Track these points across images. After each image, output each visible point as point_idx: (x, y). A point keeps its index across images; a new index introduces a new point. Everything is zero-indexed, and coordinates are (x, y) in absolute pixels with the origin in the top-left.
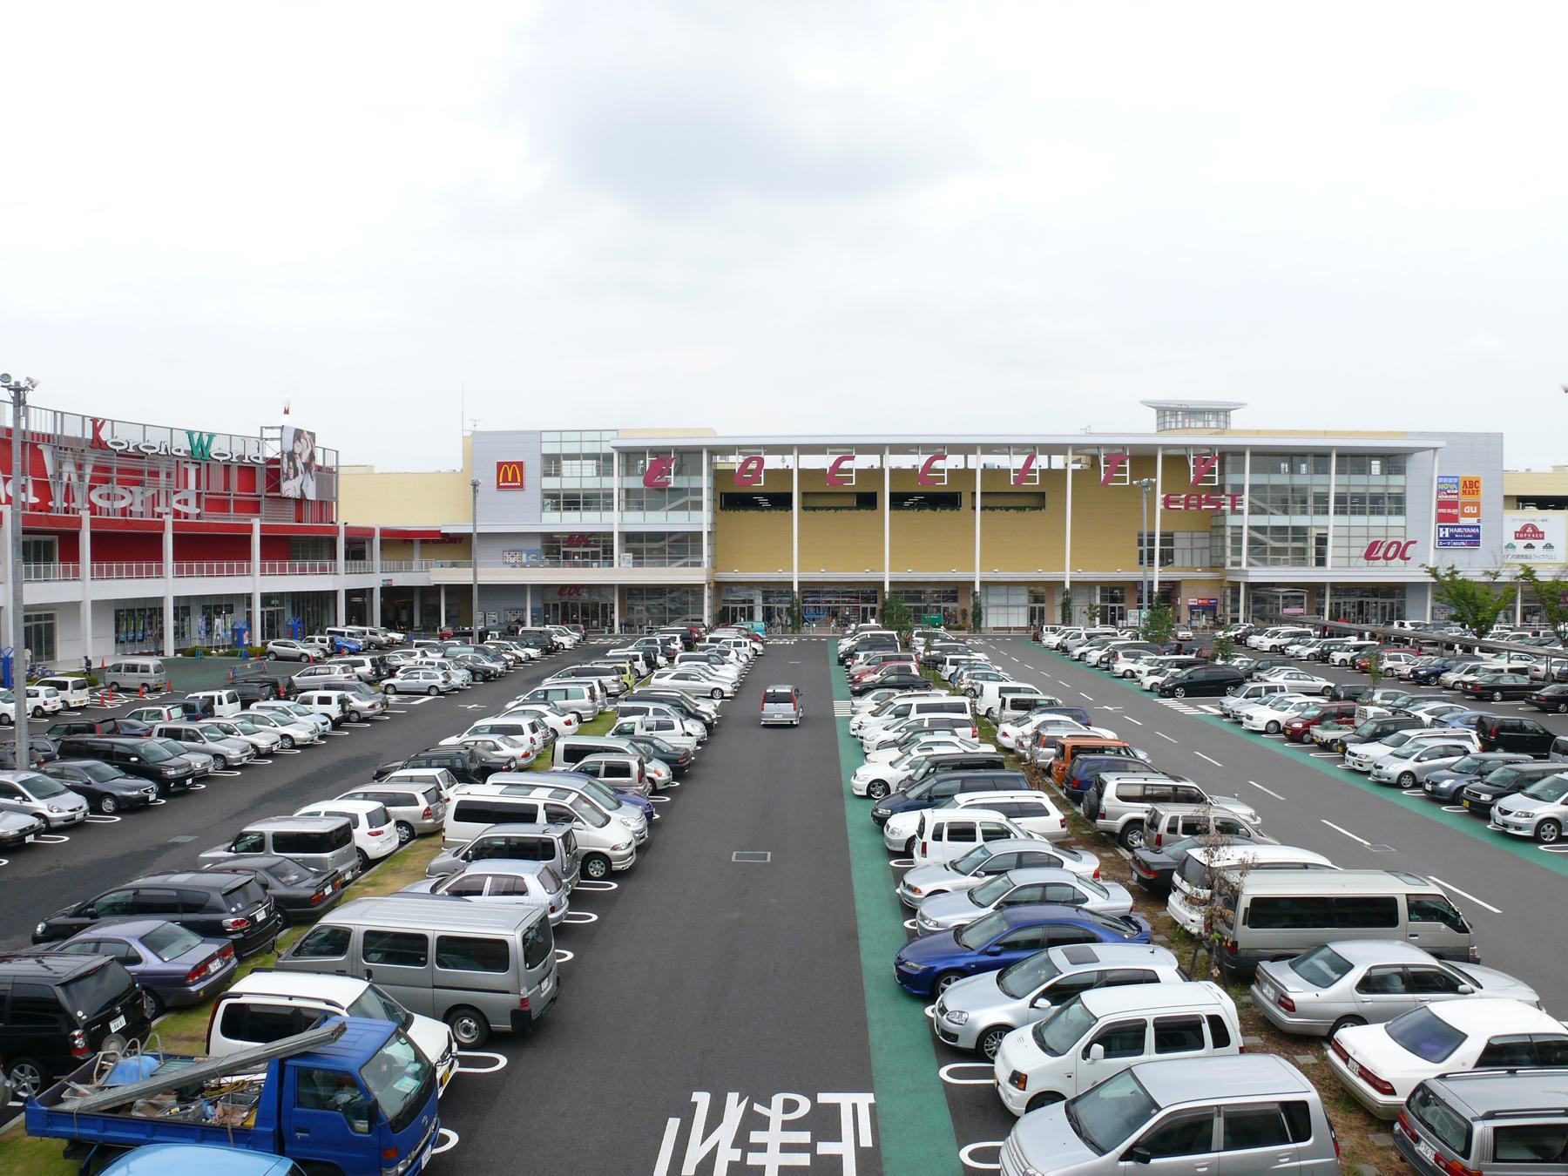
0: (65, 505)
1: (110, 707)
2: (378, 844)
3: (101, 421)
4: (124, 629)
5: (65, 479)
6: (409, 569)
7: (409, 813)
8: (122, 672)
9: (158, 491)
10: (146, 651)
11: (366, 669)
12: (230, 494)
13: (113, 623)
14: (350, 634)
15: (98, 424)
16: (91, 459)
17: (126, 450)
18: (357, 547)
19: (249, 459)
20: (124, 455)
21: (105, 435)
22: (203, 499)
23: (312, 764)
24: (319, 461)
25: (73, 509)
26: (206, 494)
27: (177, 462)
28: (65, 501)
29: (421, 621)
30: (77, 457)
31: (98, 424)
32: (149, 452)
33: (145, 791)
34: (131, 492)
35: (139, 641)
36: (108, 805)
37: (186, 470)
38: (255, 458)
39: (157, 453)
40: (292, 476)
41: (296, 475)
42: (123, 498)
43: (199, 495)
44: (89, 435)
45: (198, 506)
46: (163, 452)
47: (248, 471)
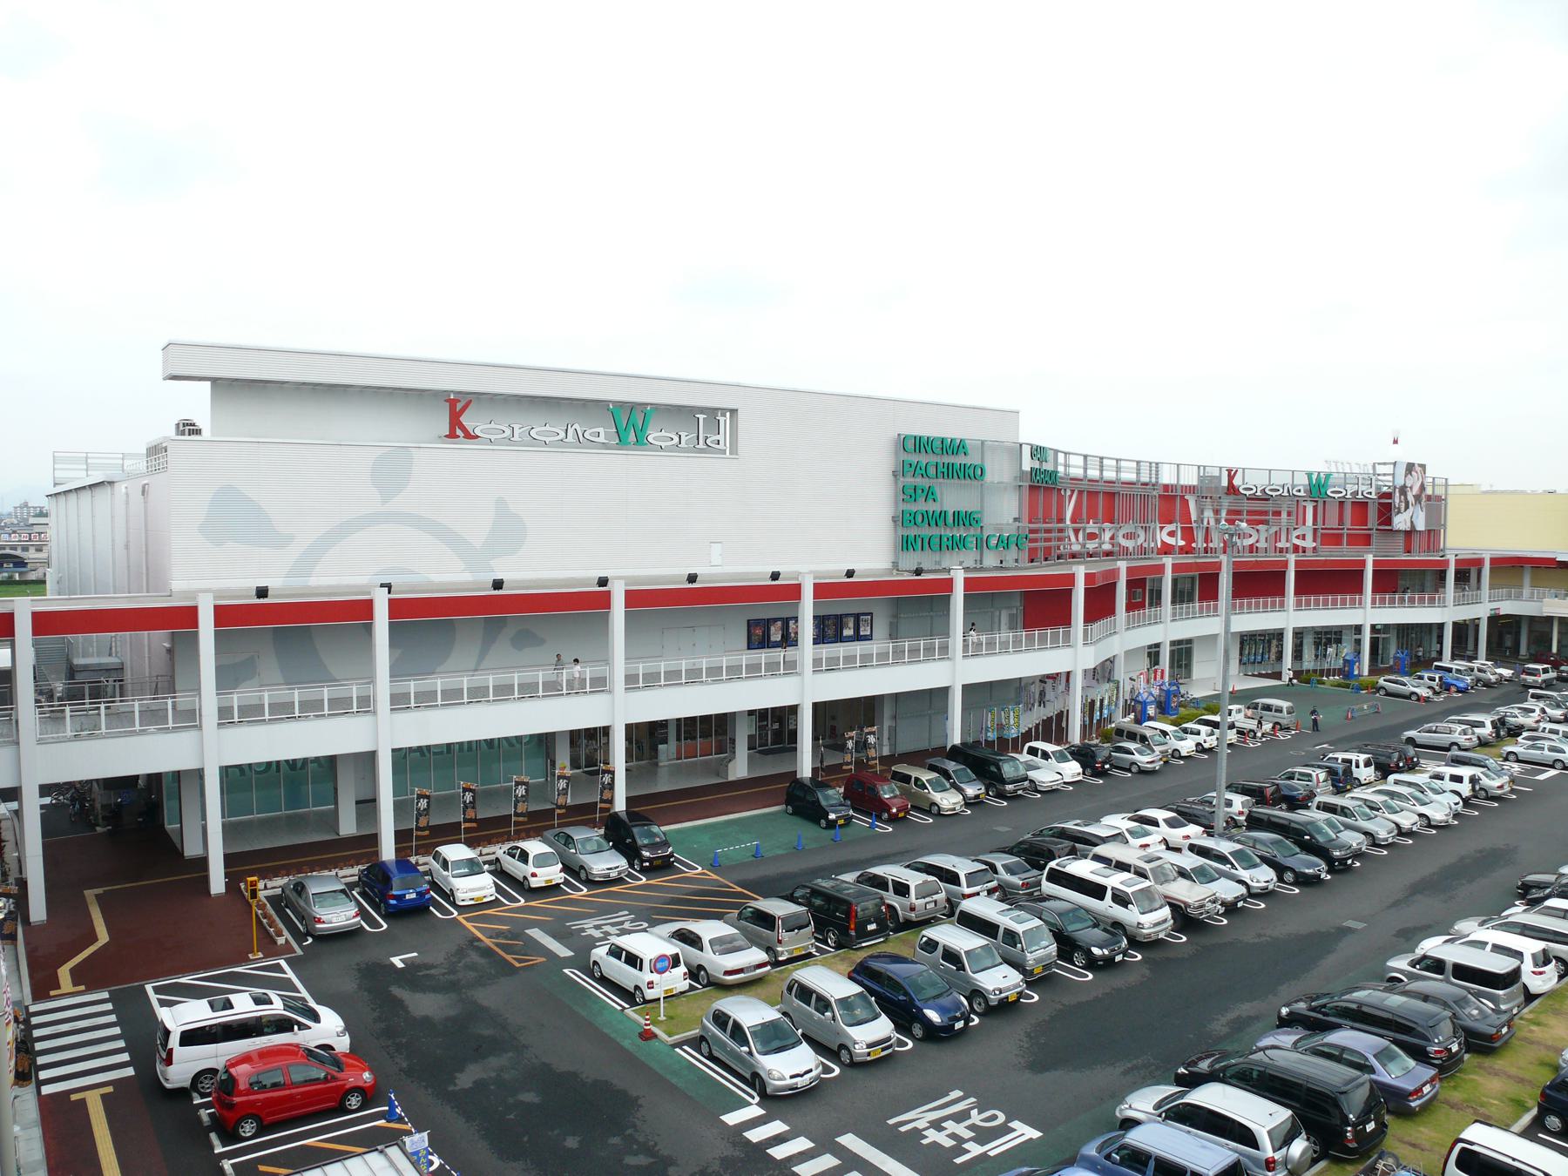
0: (1205, 545)
1: (1252, 745)
2: (1540, 983)
3: (1234, 470)
4: (1247, 652)
5: (1205, 523)
6: (1519, 597)
7: (1562, 951)
8: (1259, 710)
9: (1280, 529)
10: (1264, 672)
11: (1487, 731)
12: (1343, 529)
13: (1239, 646)
14: (1458, 671)
15: (1233, 473)
16: (1226, 503)
17: (1254, 494)
18: (1467, 573)
19: (1362, 495)
20: (1253, 498)
21: (1237, 482)
22: (1319, 534)
23: (1449, 853)
24: (1429, 491)
25: (1211, 548)
26: (1322, 529)
27: (1298, 501)
28: (1205, 542)
29: (1528, 649)
30: (1216, 504)
31: (1233, 473)
32: (1274, 494)
33: (1319, 870)
34: (1258, 530)
35: (1258, 663)
36: (1289, 876)
37: (1305, 507)
38: (1368, 493)
39: (1280, 495)
40: (1403, 509)
41: (1407, 507)
42: (1251, 536)
43: (1315, 530)
44: (1225, 483)
45: (1315, 541)
46: (1286, 494)
47: (1361, 506)
